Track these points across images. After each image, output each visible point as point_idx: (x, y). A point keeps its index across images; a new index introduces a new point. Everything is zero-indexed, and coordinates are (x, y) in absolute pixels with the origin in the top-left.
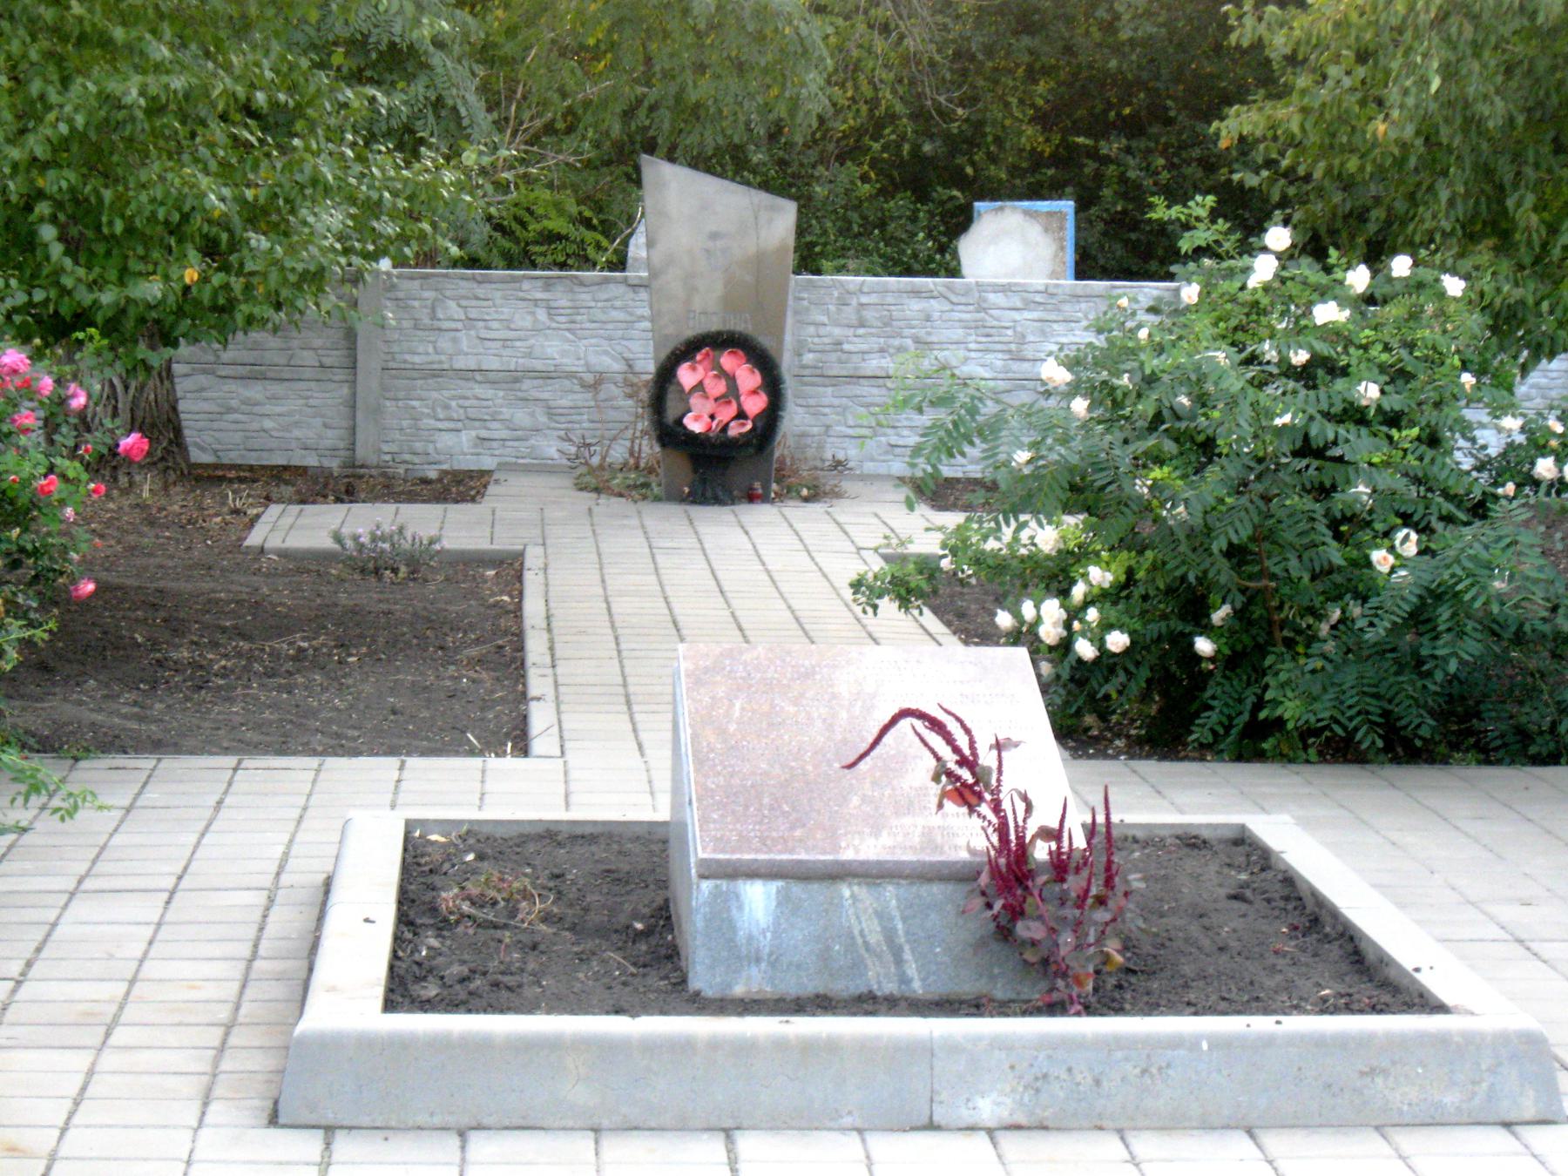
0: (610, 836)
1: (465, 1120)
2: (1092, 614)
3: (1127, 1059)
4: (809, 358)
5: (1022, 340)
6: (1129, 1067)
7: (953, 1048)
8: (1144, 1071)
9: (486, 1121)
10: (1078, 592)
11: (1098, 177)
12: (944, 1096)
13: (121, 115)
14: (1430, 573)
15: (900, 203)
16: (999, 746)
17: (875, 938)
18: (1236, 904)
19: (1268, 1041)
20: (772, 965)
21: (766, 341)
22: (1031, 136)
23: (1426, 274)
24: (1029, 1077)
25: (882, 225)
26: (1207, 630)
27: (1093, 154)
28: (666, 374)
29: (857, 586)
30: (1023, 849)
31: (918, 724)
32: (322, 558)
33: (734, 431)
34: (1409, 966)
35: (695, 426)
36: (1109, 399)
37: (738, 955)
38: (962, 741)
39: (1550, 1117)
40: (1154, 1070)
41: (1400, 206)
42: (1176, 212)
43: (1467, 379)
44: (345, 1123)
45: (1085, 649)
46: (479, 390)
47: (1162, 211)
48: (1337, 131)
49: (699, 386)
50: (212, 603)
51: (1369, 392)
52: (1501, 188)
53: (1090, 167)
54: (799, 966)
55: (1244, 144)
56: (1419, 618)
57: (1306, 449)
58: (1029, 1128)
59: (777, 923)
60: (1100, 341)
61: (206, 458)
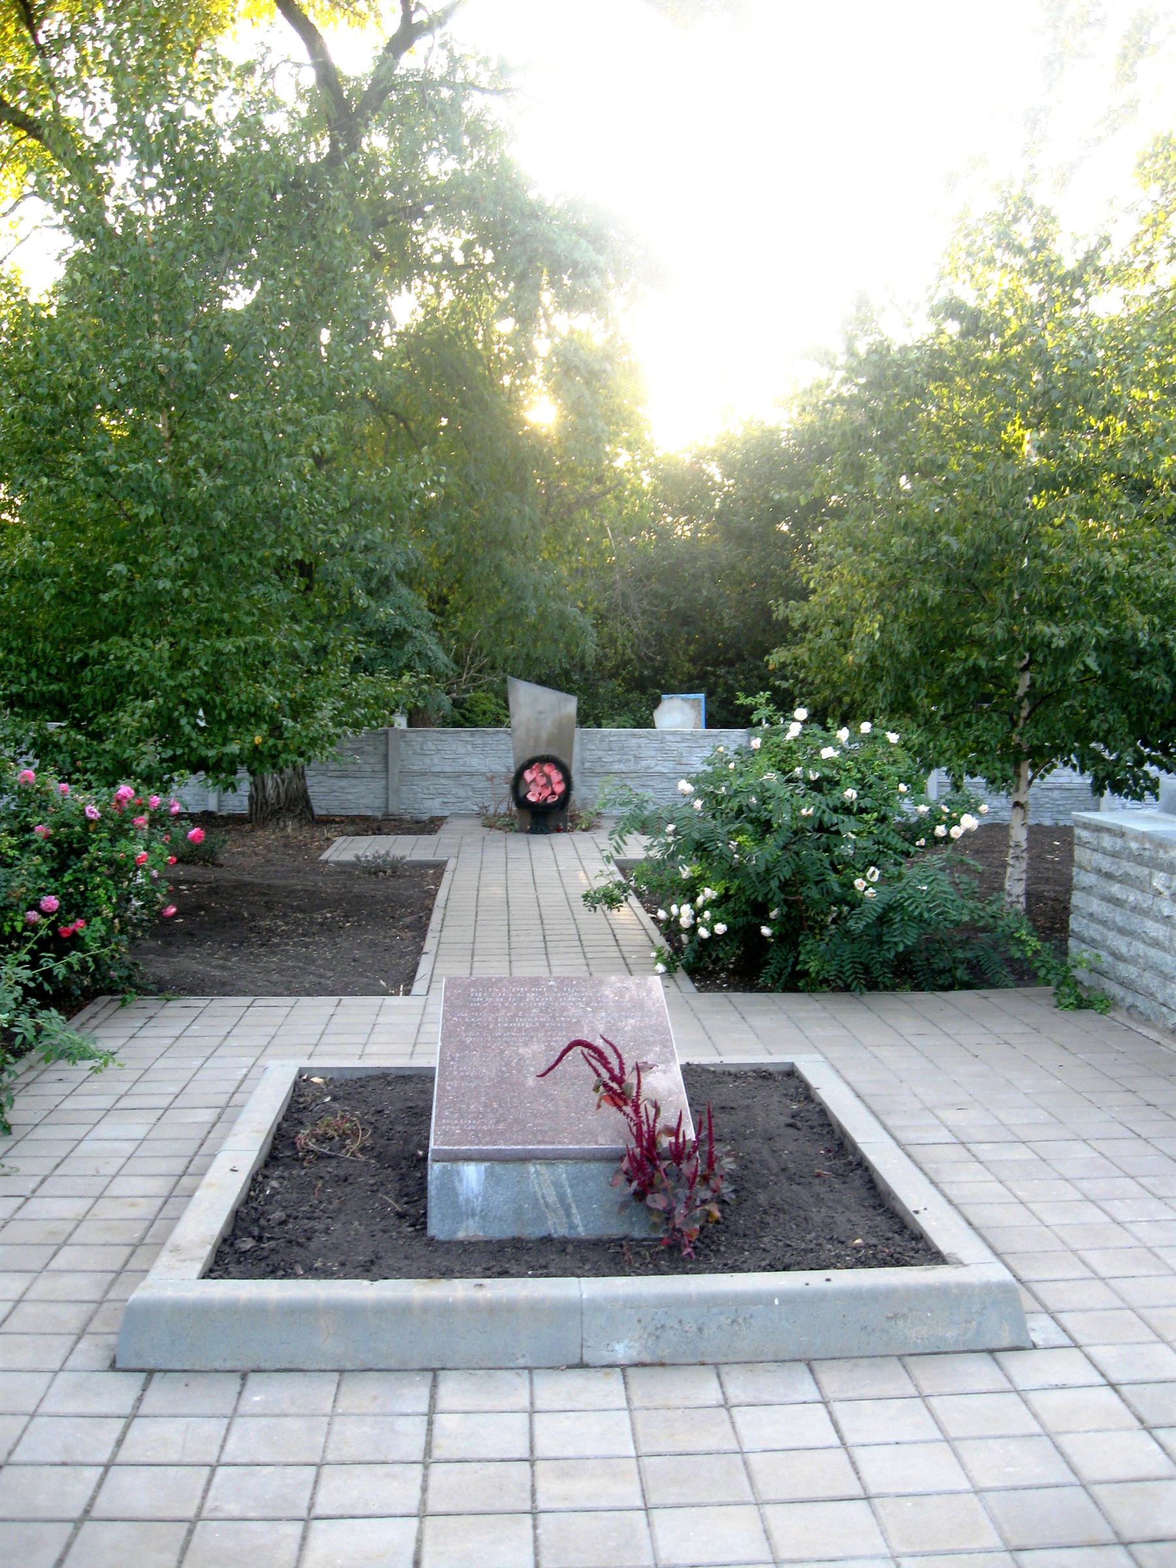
0: (420, 1076)
1: (249, 1365)
2: (707, 914)
3: (721, 1313)
4: (587, 765)
5: (681, 755)
6: (722, 1318)
7: (596, 1306)
8: (734, 1321)
9: (264, 1365)
10: (700, 900)
11: (716, 683)
12: (590, 1343)
13: (224, 658)
14: (887, 895)
15: (635, 695)
16: (638, 1069)
17: (552, 1199)
18: (791, 1131)
19: (821, 1297)
20: (483, 1218)
21: (564, 760)
22: (688, 667)
23: (878, 732)
24: (651, 1328)
25: (627, 704)
26: (768, 922)
27: (714, 674)
28: (519, 776)
29: (585, 897)
30: (653, 1140)
31: (586, 1050)
32: (354, 865)
33: (550, 800)
34: (911, 1207)
35: (532, 798)
36: (712, 799)
37: (460, 1212)
38: (614, 1063)
39: (1020, 1344)
40: (740, 1320)
41: (858, 696)
42: (750, 701)
43: (903, 787)
44: (163, 1367)
45: (703, 933)
46: (443, 781)
47: (742, 700)
48: (826, 660)
49: (534, 780)
50: (292, 893)
51: (851, 793)
52: (908, 687)
53: (712, 680)
54: (501, 1219)
55: (783, 665)
56: (883, 919)
57: (821, 828)
58: (652, 1365)
59: (485, 1188)
60: (709, 769)
61: (323, 812)
